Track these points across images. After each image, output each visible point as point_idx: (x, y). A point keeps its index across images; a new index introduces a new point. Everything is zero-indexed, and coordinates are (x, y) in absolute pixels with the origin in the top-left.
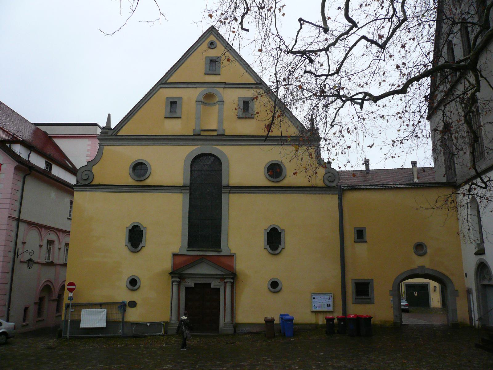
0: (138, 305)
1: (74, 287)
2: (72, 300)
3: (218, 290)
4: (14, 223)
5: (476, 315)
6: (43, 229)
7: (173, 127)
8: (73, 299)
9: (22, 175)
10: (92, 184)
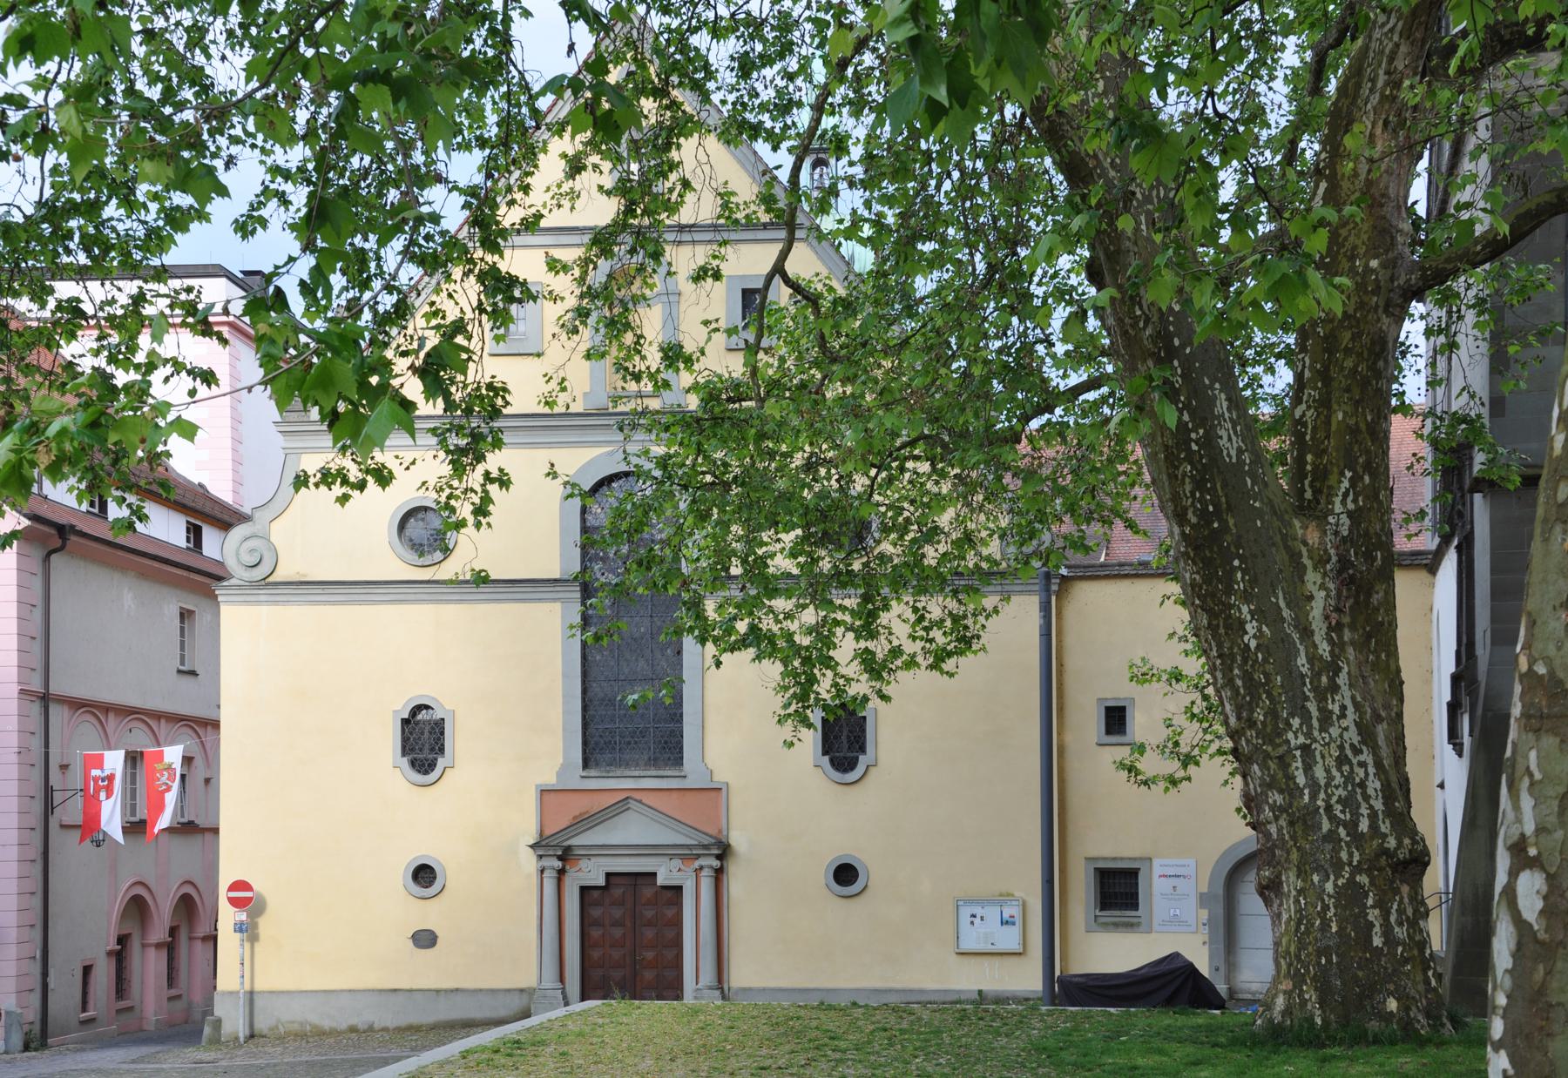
4: (36, 709)
6: (111, 716)
9: (37, 554)
10: (270, 579)
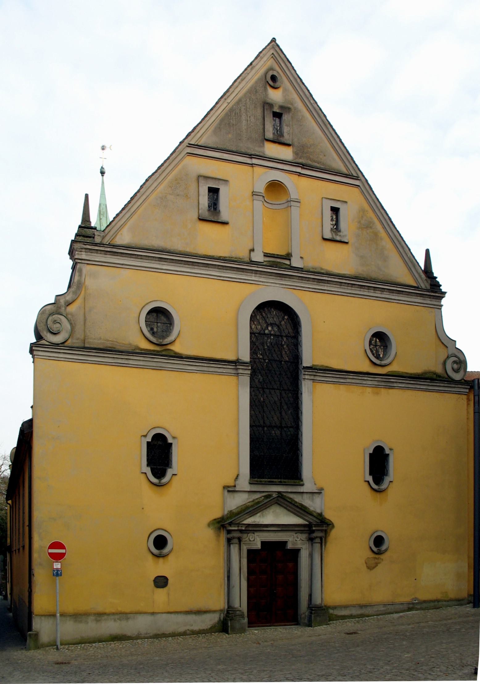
0: (170, 582)
1: (51, 551)
2: (61, 575)
3: (296, 552)
5: (58, 581)
7: (212, 240)
8: (61, 573)
